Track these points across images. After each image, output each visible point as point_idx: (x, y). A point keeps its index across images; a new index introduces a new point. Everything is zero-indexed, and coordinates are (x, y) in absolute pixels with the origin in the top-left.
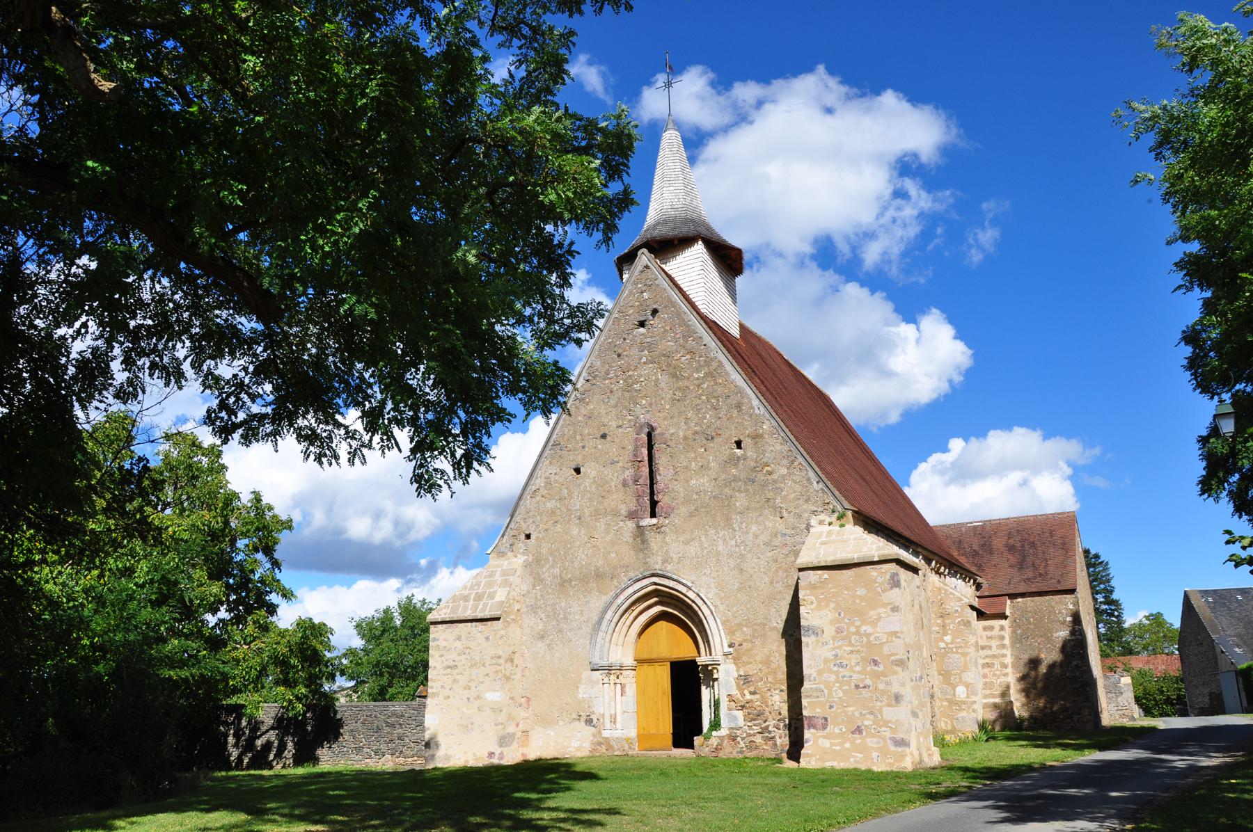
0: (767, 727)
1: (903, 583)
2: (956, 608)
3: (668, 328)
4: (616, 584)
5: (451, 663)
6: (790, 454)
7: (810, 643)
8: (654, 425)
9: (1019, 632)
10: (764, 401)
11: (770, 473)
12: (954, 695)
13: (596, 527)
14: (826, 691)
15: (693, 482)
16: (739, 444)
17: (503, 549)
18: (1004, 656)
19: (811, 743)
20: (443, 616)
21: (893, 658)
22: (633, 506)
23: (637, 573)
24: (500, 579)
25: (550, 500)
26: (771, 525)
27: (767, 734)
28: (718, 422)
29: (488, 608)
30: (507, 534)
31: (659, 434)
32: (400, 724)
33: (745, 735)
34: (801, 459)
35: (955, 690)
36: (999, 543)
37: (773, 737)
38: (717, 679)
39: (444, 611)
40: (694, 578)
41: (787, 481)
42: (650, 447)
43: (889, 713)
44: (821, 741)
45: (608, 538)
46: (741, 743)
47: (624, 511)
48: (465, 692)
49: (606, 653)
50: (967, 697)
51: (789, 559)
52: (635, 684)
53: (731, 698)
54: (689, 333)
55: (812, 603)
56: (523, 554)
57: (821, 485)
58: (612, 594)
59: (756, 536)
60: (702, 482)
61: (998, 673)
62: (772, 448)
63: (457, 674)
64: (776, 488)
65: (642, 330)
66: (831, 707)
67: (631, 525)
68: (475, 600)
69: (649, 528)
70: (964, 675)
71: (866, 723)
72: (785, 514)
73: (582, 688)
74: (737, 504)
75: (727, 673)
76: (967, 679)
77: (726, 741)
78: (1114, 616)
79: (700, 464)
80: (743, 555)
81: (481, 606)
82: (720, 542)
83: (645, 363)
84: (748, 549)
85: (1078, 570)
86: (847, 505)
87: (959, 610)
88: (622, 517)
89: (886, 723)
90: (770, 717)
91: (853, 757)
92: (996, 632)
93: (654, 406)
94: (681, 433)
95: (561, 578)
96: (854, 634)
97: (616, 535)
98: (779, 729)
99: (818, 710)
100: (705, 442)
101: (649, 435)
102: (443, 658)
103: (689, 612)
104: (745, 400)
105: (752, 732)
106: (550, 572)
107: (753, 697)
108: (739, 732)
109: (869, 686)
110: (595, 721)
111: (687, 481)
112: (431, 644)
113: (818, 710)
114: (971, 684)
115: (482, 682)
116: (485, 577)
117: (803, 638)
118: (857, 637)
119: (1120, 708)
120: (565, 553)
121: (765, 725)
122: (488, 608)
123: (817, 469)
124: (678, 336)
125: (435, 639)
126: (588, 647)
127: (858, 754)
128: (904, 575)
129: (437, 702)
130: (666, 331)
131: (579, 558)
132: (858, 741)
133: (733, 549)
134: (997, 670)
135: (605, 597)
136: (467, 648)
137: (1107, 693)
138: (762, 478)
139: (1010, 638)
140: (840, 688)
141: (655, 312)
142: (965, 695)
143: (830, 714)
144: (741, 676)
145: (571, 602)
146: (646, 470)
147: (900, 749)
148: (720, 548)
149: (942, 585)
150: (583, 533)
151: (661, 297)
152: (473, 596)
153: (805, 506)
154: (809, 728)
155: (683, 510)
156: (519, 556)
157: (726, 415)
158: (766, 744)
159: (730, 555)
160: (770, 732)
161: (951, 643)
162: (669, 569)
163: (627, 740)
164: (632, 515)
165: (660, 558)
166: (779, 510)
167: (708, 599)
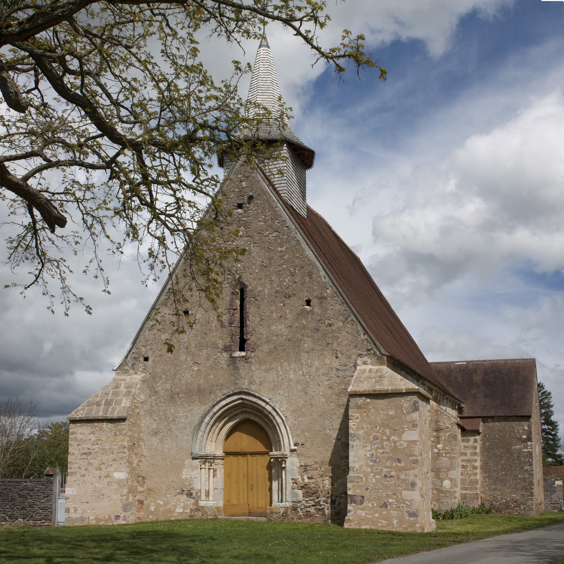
0: (319, 502)
1: (421, 408)
2: (448, 425)
3: (260, 211)
4: (213, 398)
5: (87, 451)
6: (345, 312)
7: (355, 445)
8: (246, 283)
9: (487, 444)
10: (329, 273)
11: (330, 325)
12: (442, 486)
13: (200, 355)
14: (364, 479)
15: (273, 327)
16: (308, 303)
17: (126, 367)
18: (475, 461)
19: (352, 513)
20: (80, 416)
21: (411, 458)
22: (228, 341)
23: (229, 390)
24: (125, 390)
25: (165, 333)
26: (329, 362)
27: (319, 507)
28: (294, 285)
29: (116, 411)
30: (129, 356)
31: (250, 290)
32: (31, 496)
33: (303, 507)
34: (353, 317)
35: (442, 483)
36: (477, 379)
37: (324, 509)
38: (285, 468)
39: (81, 412)
40: (271, 396)
41: (342, 332)
42: (242, 300)
43: (407, 494)
44: (359, 511)
45: (208, 365)
46: (300, 512)
47: (221, 344)
48: (97, 472)
49: (204, 446)
50: (451, 488)
51: (340, 387)
52: (223, 469)
53: (295, 481)
54: (276, 216)
55: (357, 418)
56: (142, 372)
57: (366, 336)
58: (210, 404)
59: (318, 369)
60: (280, 328)
61: (470, 472)
62: (333, 307)
63: (91, 459)
64: (334, 336)
65: (240, 211)
66: (367, 489)
67: (226, 355)
68: (105, 405)
69: (239, 359)
70: (450, 472)
71: (390, 500)
72: (339, 355)
73: (185, 471)
74: (305, 346)
75: (292, 464)
76: (451, 476)
77: (289, 511)
78: (551, 434)
79: (280, 315)
80: (308, 382)
81: (110, 410)
82: (292, 372)
83: (241, 236)
84: (311, 378)
85: (533, 402)
86: (383, 351)
87: (450, 427)
88: (219, 350)
89: (404, 501)
90: (322, 495)
91: (380, 522)
92: (471, 443)
93: (246, 269)
94: (266, 291)
95: (171, 391)
96: (386, 440)
97: (214, 362)
98: (327, 503)
99: (358, 491)
100: (283, 299)
101: (242, 291)
102: (80, 447)
103: (266, 419)
104: (315, 270)
105: (308, 505)
106: (162, 386)
107: (310, 481)
108: (299, 505)
109: (394, 476)
110: (194, 495)
111: (269, 327)
112: (70, 436)
113: (358, 491)
114: (453, 479)
115: (111, 465)
116: (113, 389)
117: (350, 442)
118: (388, 443)
119: (553, 502)
120: (174, 373)
121: (317, 500)
122: (116, 411)
123: (364, 325)
124: (267, 218)
125: (73, 433)
126: (190, 442)
127: (384, 521)
128: (421, 403)
129: (75, 479)
130: (258, 213)
131: (185, 377)
132: (384, 513)
133: (301, 377)
134: (470, 470)
135: (204, 407)
136: (99, 440)
137: (545, 491)
138: (324, 328)
139: (481, 448)
140: (374, 477)
141: (251, 198)
142: (449, 487)
143: (366, 494)
144: (302, 466)
145: (178, 409)
146: (238, 315)
147: (412, 519)
148: (291, 376)
149: (439, 409)
150: (189, 359)
151: (256, 187)
152: (103, 402)
153: (354, 351)
154: (351, 503)
155: (266, 348)
156: (139, 373)
157: (300, 281)
158: (317, 513)
159: (298, 382)
160: (321, 505)
161: (442, 450)
162: (253, 389)
163: (218, 508)
164: (227, 349)
165: (246, 381)
166: (335, 351)
167: (281, 411)
